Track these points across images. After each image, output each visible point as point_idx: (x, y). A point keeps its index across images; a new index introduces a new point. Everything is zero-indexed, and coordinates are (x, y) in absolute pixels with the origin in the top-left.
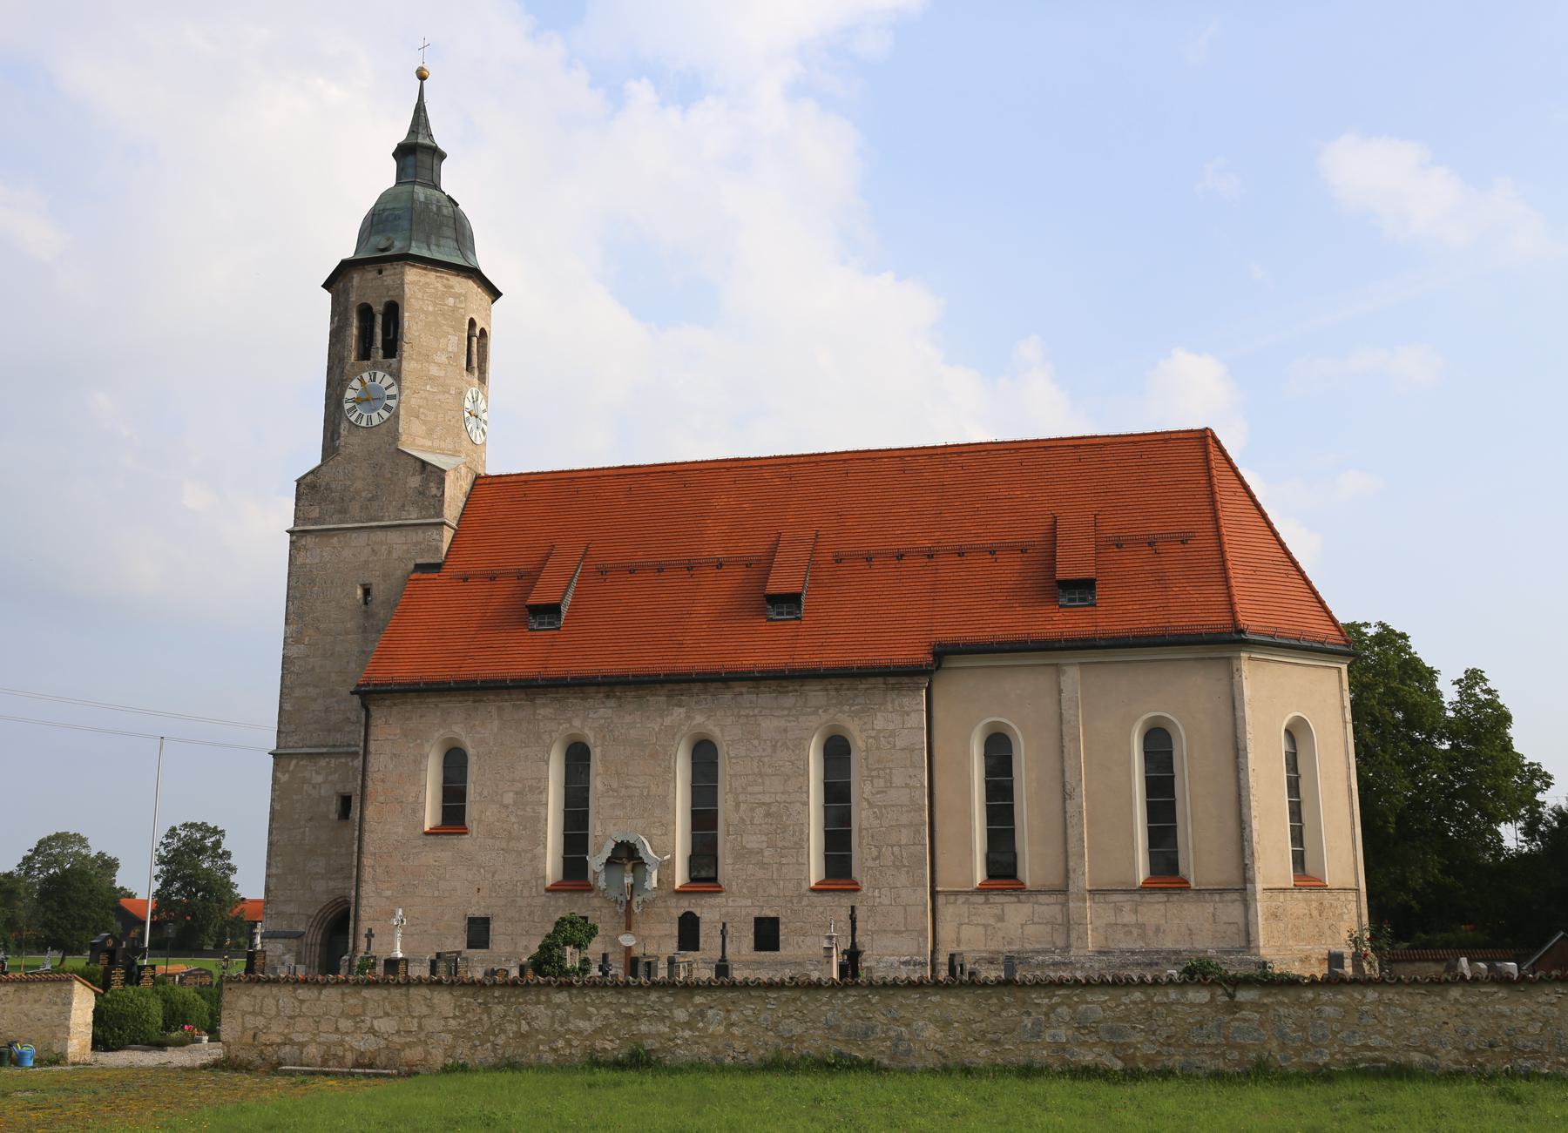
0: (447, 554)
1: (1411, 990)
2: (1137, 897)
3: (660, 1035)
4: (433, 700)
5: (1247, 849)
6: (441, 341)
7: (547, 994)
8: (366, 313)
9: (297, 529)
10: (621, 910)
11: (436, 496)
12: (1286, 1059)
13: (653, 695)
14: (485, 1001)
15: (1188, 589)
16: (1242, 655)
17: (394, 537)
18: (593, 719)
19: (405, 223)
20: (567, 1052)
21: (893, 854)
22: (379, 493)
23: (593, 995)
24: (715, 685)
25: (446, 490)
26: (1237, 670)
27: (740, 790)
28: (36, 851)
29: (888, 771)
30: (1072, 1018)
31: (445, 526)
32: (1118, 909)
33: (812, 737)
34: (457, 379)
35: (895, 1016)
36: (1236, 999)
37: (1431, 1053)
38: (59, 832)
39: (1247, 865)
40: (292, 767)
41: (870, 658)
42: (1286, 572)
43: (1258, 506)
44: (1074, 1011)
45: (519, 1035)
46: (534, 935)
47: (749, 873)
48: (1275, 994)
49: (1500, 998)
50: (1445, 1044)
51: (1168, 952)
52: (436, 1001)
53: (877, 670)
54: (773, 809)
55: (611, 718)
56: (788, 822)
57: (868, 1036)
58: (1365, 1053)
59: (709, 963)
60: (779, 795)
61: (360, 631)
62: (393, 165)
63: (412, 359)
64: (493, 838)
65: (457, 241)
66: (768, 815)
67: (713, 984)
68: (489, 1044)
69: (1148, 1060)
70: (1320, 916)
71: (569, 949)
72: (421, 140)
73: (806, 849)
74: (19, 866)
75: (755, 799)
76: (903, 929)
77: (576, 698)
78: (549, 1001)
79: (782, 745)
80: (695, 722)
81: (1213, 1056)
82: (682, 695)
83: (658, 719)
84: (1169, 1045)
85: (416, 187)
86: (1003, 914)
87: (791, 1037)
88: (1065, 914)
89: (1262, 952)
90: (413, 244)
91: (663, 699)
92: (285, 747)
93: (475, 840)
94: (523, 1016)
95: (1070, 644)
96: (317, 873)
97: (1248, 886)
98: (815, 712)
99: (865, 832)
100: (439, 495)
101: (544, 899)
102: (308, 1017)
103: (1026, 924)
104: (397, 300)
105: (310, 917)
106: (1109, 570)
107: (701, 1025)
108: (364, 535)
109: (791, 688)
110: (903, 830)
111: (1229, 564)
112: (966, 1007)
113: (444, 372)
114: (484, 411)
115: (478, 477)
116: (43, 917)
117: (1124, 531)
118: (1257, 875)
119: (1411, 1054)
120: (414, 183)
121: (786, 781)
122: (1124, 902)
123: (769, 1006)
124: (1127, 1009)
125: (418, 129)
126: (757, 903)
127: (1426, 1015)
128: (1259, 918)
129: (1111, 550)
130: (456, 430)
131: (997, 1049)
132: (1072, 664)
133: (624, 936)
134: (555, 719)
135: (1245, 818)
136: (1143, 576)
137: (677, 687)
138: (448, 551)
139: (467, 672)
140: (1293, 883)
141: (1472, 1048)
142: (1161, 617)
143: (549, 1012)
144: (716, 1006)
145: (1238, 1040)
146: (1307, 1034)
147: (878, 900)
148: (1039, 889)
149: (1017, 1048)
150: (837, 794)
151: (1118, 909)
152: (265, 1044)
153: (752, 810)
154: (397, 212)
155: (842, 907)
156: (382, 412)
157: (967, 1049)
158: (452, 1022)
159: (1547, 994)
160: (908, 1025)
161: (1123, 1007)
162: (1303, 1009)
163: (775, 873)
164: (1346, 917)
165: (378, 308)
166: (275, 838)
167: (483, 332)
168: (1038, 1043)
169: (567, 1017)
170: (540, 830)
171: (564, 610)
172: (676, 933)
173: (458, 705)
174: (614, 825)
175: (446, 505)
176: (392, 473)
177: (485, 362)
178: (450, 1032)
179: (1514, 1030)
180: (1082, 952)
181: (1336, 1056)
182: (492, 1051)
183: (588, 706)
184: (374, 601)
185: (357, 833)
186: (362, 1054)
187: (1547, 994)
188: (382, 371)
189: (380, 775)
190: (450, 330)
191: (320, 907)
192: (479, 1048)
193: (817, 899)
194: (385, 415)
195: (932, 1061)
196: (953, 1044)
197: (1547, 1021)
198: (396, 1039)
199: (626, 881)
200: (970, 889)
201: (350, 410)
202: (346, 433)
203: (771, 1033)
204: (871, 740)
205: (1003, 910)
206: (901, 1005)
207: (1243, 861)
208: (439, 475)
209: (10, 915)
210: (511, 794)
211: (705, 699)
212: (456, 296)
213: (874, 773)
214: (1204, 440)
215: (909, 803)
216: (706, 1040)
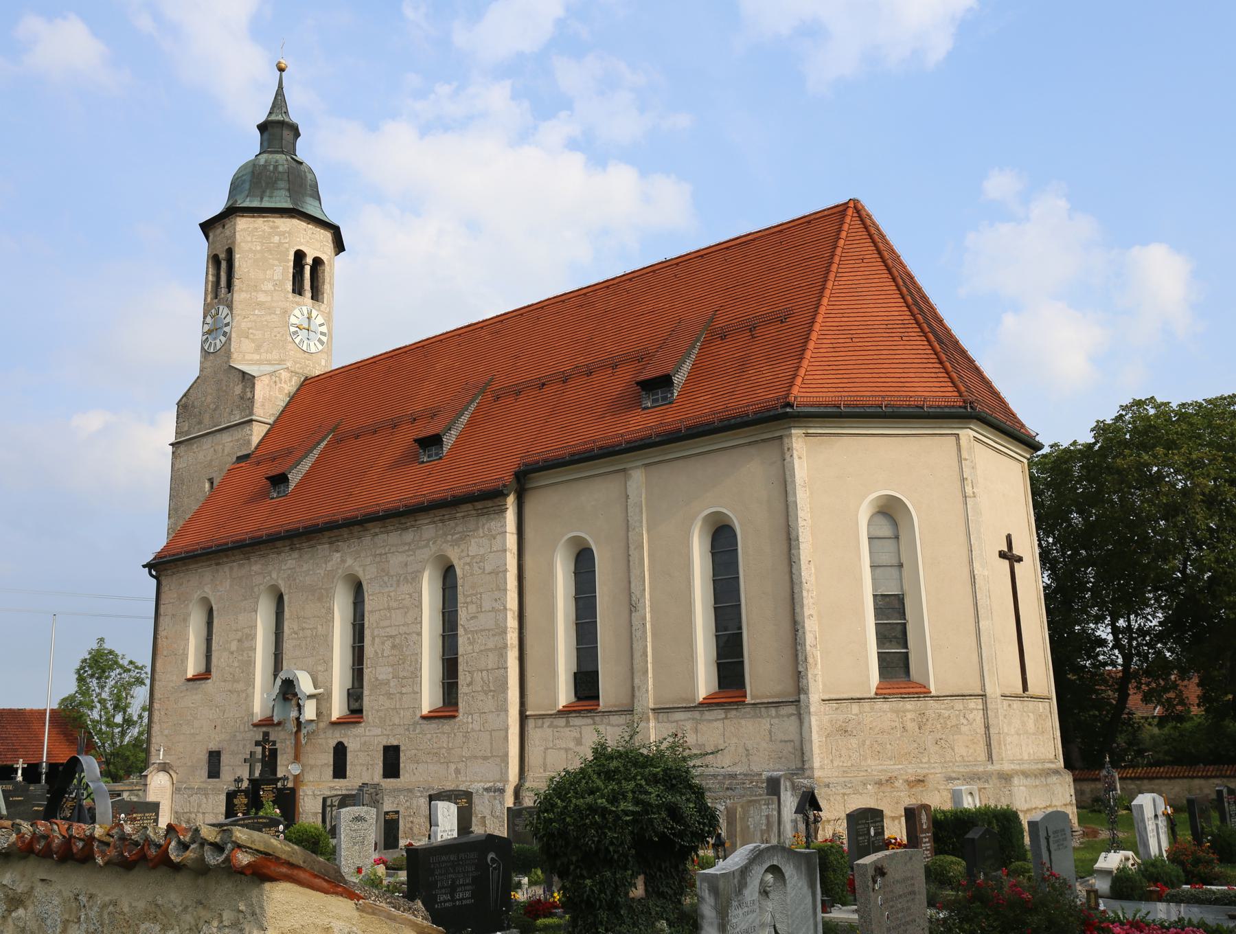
2: (697, 715)
4: (193, 566)
5: (800, 654)
6: (268, 272)
16: (793, 431)
26: (789, 449)
27: (375, 625)
39: (800, 672)
54: (397, 641)
55: (294, 568)
56: (407, 653)
64: (225, 681)
65: (289, 190)
80: (347, 565)
82: (338, 541)
83: (324, 566)
89: (817, 774)
97: (802, 697)
98: (427, 546)
101: (252, 733)
110: (490, 654)
122: (685, 720)
126: (385, 732)
130: (281, 343)
132: (637, 467)
135: (798, 618)
153: (383, 643)
155: (444, 733)
164: (964, 729)
165: (222, 256)
172: (332, 763)
190: (276, 262)
194: (223, 339)
199: (291, 715)
207: (797, 668)
212: (282, 234)
213: (469, 599)
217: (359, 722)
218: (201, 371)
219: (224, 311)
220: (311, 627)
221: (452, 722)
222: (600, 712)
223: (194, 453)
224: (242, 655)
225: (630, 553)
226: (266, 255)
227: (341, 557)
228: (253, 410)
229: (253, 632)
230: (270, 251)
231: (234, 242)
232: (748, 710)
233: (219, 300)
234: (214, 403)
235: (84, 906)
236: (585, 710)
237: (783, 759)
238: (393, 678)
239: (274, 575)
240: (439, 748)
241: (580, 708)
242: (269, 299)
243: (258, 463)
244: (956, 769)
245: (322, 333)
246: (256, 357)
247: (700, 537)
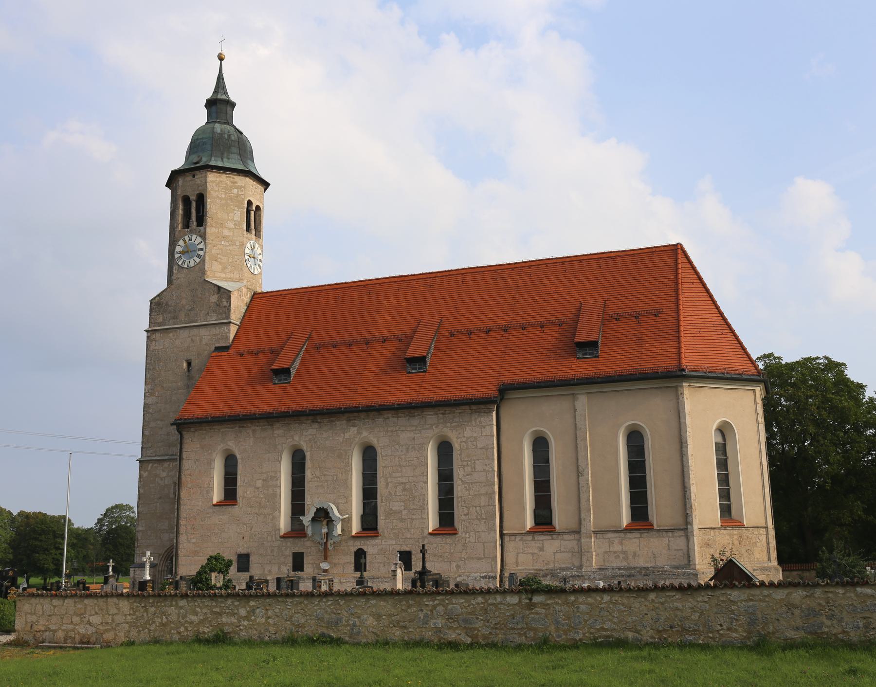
0: (233, 340)
1: (628, 595)
2: (622, 535)
3: (232, 624)
4: (217, 427)
5: (688, 504)
6: (230, 215)
7: (176, 601)
8: (186, 200)
9: (150, 329)
10: (322, 548)
12: (559, 636)
13: (340, 420)
14: (145, 605)
15: (655, 344)
16: (684, 384)
17: (203, 332)
19: (209, 147)
20: (186, 634)
21: (476, 511)
22: (195, 306)
23: (199, 601)
24: (373, 413)
25: (231, 302)
26: (681, 394)
27: (388, 475)
28: (105, 515)
29: (473, 462)
30: (445, 613)
31: (231, 324)
32: (611, 543)
33: (429, 442)
35: (352, 612)
36: (533, 601)
37: (638, 632)
38: (118, 504)
39: (688, 514)
40: (149, 468)
41: (463, 394)
42: (721, 331)
43: (707, 290)
44: (446, 609)
45: (162, 624)
46: (274, 564)
47: (394, 525)
48: (554, 598)
49: (677, 599)
50: (646, 627)
51: (641, 569)
52: (121, 605)
53: (465, 402)
57: (338, 624)
58: (602, 632)
59: (371, 579)
60: (410, 478)
61: (186, 387)
62: (205, 112)
63: (213, 227)
65: (240, 155)
66: (404, 490)
67: (258, 594)
68: (147, 630)
69: (485, 637)
70: (740, 544)
71: (213, 575)
72: (220, 96)
73: (426, 510)
74: (96, 524)
75: (397, 480)
76: (483, 557)
77: (296, 423)
78: (177, 604)
79: (412, 448)
80: (363, 436)
81: (520, 635)
82: (355, 420)
83: (342, 435)
84: (496, 628)
85: (217, 124)
86: (543, 547)
87: (298, 625)
88: (579, 546)
89: (698, 567)
90: (213, 159)
91: (344, 422)
92: (145, 457)
93: (241, 508)
94: (164, 613)
95: (579, 382)
96: (164, 529)
97: (689, 526)
98: (431, 428)
99: (460, 499)
100: (227, 306)
101: (279, 542)
102: (58, 615)
103: (556, 552)
104: (203, 193)
105: (160, 555)
106: (609, 335)
107: (253, 618)
108: (187, 331)
109: (416, 414)
110: (482, 497)
111: (682, 328)
112: (389, 606)
113: (232, 233)
114: (260, 254)
115: (255, 294)
116: (105, 554)
117: (621, 310)
118: (694, 520)
119: (628, 633)
120: (215, 122)
121: (414, 469)
123: (288, 607)
124: (474, 608)
125: (218, 90)
126: (398, 543)
127: (636, 610)
128: (696, 546)
129: (612, 322)
131: (405, 631)
133: (323, 564)
135: (687, 485)
136: (629, 337)
137: (351, 415)
138: (234, 338)
139: (235, 411)
140: (720, 524)
141: (661, 629)
142: (636, 363)
143: (177, 611)
144: (261, 607)
145: (533, 625)
146: (571, 622)
147: (468, 540)
148: (564, 531)
149: (415, 630)
150: (446, 478)
151: (611, 543)
152: (37, 631)
153: (396, 487)
154: (204, 140)
155: (447, 544)
156: (196, 258)
157: (390, 631)
158: (128, 617)
159: (703, 596)
160: (359, 617)
161: (472, 606)
162: (569, 607)
163: (409, 524)
164: (758, 544)
165: (193, 198)
166: (141, 509)
167: (258, 208)
168: (426, 627)
169: (186, 614)
171: (293, 371)
173: (231, 430)
174: (318, 498)
175: (232, 312)
176: (201, 294)
177: (260, 225)
178: (127, 623)
179: (684, 618)
180: (589, 569)
181: (586, 635)
182: (148, 634)
184: (193, 370)
185: (176, 506)
186: (84, 636)
187: (703, 596)
188: (196, 235)
189: (188, 472)
190: (235, 208)
191: (165, 549)
192: (142, 632)
193: (433, 539)
194: (198, 260)
195: (371, 638)
196: (382, 628)
197: (703, 612)
198: (101, 627)
199: (323, 531)
200: (524, 532)
201: (178, 258)
202: (176, 271)
203: (288, 622)
204: (463, 444)
205: (543, 544)
206: (355, 605)
207: (686, 511)
208: (224, 294)
209: (85, 553)
210: (260, 481)
211: (368, 422)
212: (239, 188)
213: (465, 463)
214: (676, 252)
215: (485, 481)
216: (256, 626)
217: (378, 536)
221: (453, 537)
222: (557, 532)
224: (268, 490)
225: (578, 442)
226: (229, 202)
227: (357, 430)
230: (231, 199)
231: (205, 189)
232: (655, 533)
235: (754, 611)
236: (546, 531)
237: (676, 560)
238: (404, 509)
239: (296, 438)
240: (444, 552)
241: (544, 530)
242: (231, 234)
244: (756, 565)
246: (223, 275)
247: (622, 436)
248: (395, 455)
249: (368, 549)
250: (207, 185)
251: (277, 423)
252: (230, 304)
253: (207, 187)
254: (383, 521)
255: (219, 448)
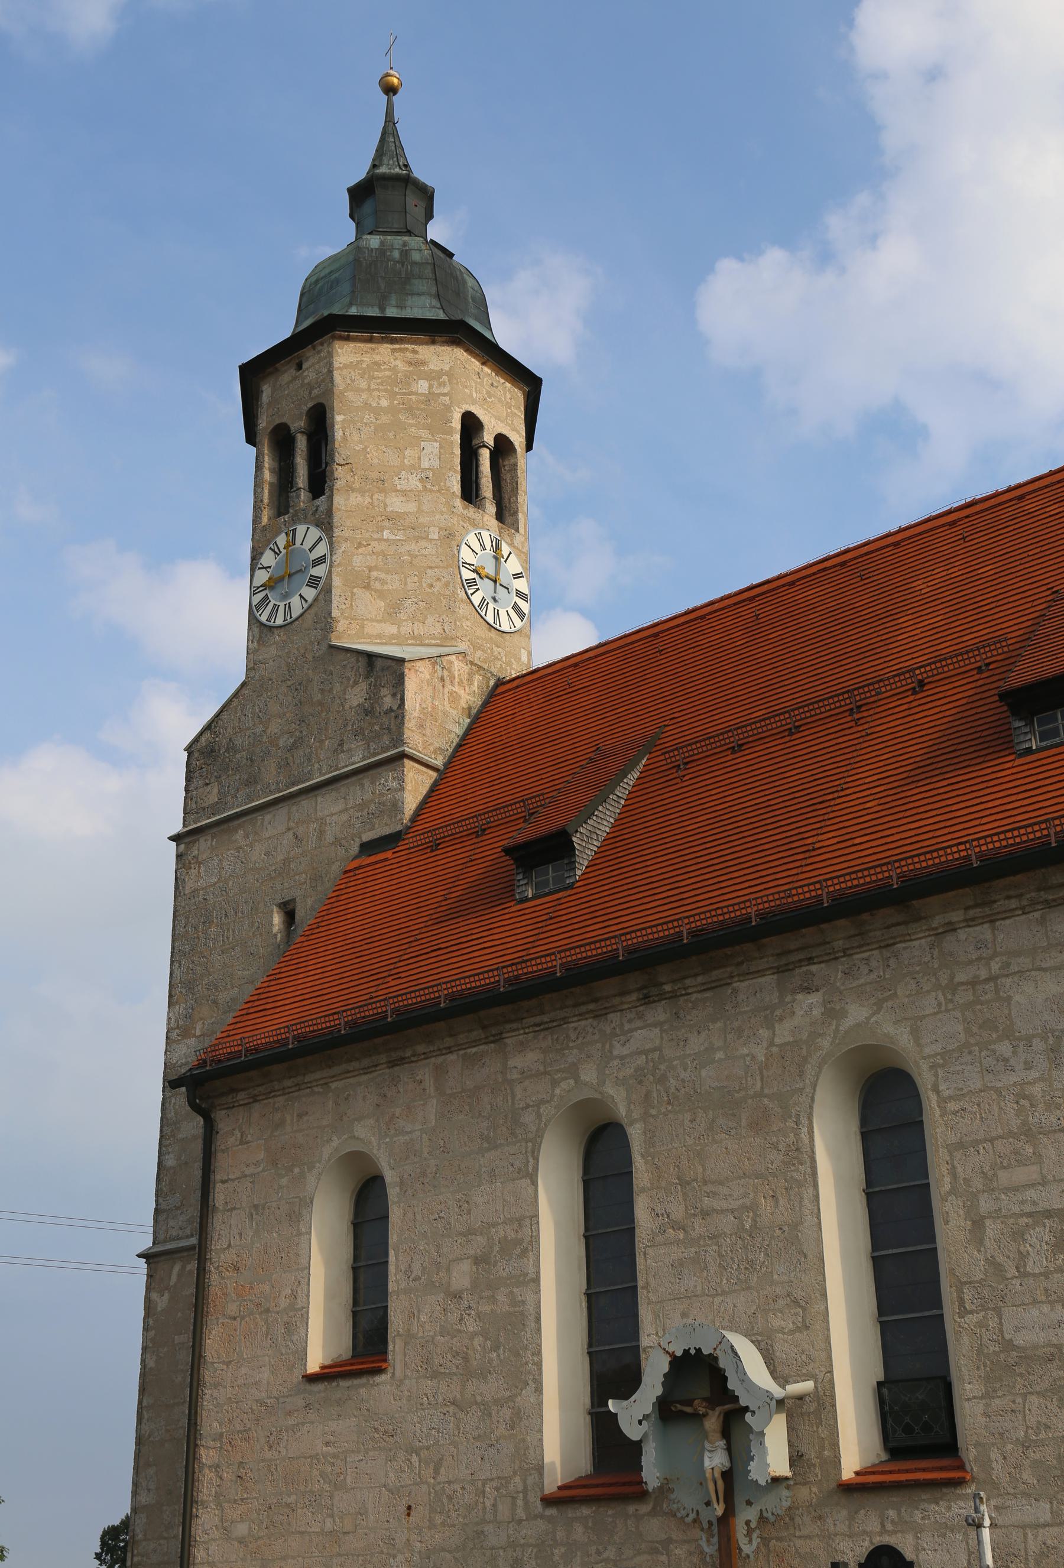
4: (318, 1075)
11: (391, 710)
18: (622, 1058)
27: (978, 1183)
31: (406, 762)
34: (442, 513)
40: (174, 1278)
47: (1032, 1420)
55: (658, 1049)
63: (353, 490)
64: (435, 1375)
65: (438, 296)
80: (848, 1022)
82: (810, 961)
83: (764, 1033)
91: (769, 979)
92: (165, 1241)
100: (395, 708)
101: (541, 1525)
134: (546, 1073)
153: (1018, 1235)
154: (333, 277)
165: (298, 424)
170: (526, 1348)
173: (365, 1078)
174: (684, 1315)
176: (322, 691)
183: (608, 1031)
188: (305, 523)
189: (229, 1257)
190: (424, 433)
194: (310, 593)
199: (707, 1464)
210: (466, 1266)
212: (434, 377)
217: (960, 1483)
218: (249, 669)
219: (307, 534)
220: (734, 1205)
223: (238, 849)
224: (493, 1300)
228: (401, 733)
229: (527, 1231)
230: (410, 409)
231: (329, 389)
233: (296, 514)
234: (291, 733)
239: (589, 1074)
242: (412, 507)
243: (435, 846)
245: (519, 594)
248: (999, 1085)
249: (918, 1549)
250: (332, 377)
251: (514, 1025)
252: (402, 700)
253: (332, 381)
254: (979, 1408)
255: (327, 1151)
